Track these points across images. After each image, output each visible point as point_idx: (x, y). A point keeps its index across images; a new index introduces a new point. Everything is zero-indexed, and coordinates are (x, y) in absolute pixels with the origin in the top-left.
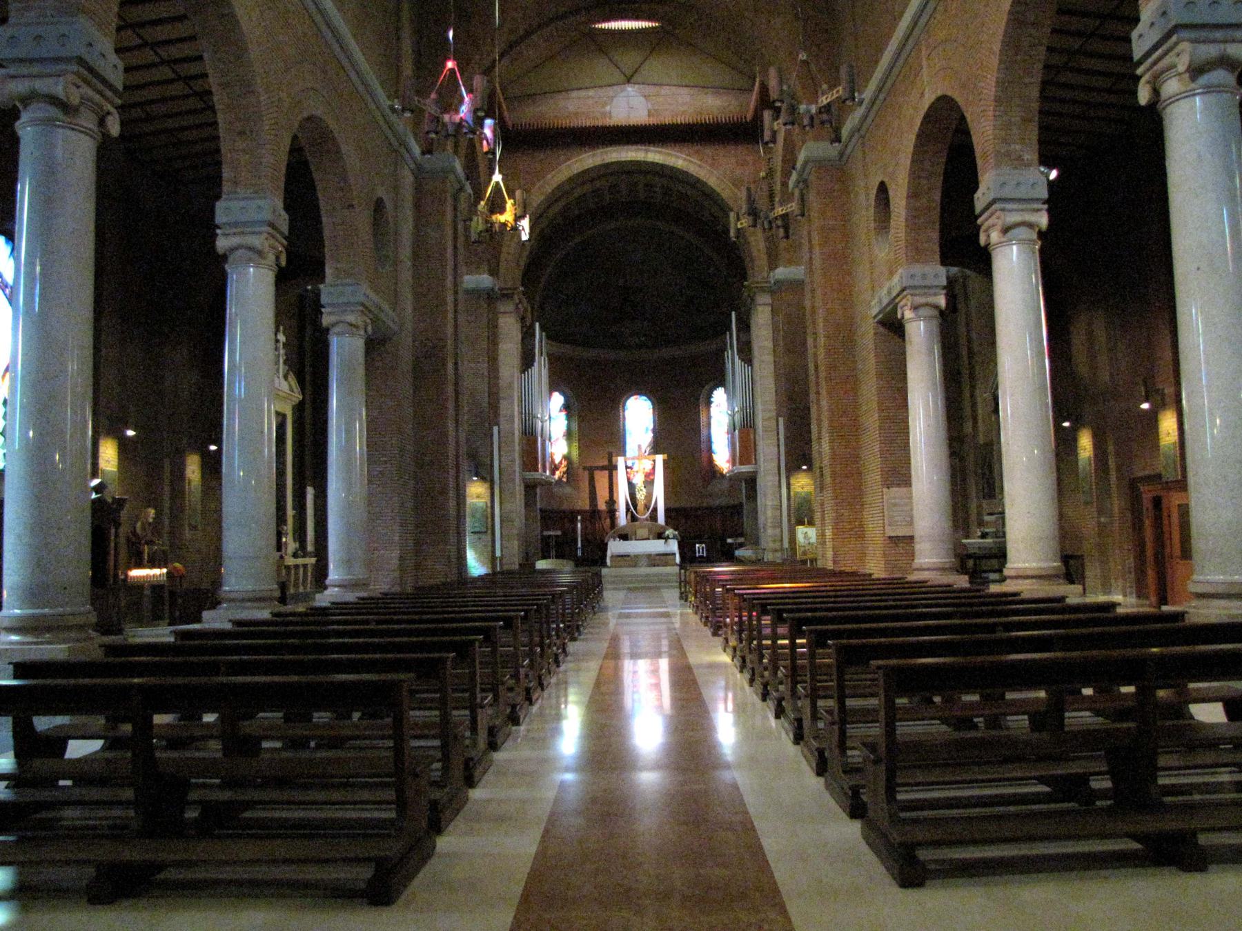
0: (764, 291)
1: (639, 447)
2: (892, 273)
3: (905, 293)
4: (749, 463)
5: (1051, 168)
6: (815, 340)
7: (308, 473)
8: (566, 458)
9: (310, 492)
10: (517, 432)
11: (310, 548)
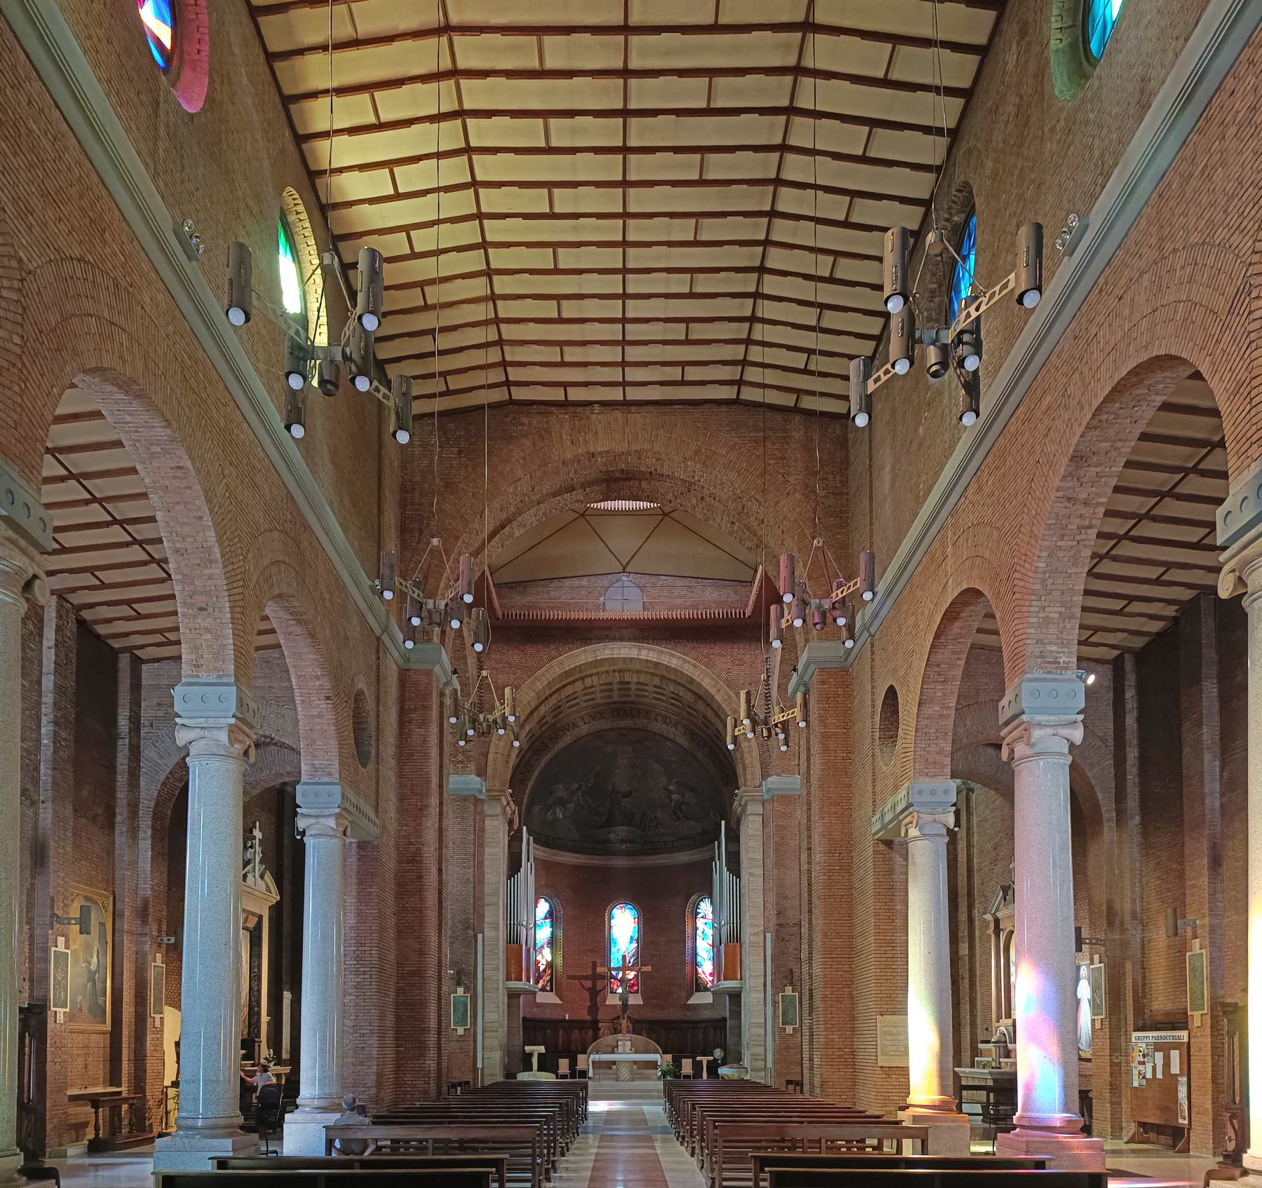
0: (755, 800)
1: (624, 957)
2: (896, 788)
3: (911, 809)
4: (735, 979)
5: (1089, 672)
6: (809, 856)
7: (285, 978)
8: (550, 965)
9: (287, 996)
10: (501, 940)
11: (285, 1055)
